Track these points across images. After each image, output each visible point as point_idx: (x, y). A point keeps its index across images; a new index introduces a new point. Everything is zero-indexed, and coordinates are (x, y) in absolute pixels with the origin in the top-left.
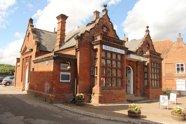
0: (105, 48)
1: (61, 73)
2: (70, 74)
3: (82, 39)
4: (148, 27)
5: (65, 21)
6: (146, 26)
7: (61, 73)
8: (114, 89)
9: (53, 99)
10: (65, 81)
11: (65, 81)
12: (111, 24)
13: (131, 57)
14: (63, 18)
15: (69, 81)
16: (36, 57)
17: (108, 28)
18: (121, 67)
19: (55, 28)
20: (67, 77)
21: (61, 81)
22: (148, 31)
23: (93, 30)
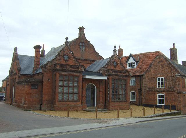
12: (71, 52)
14: (37, 48)
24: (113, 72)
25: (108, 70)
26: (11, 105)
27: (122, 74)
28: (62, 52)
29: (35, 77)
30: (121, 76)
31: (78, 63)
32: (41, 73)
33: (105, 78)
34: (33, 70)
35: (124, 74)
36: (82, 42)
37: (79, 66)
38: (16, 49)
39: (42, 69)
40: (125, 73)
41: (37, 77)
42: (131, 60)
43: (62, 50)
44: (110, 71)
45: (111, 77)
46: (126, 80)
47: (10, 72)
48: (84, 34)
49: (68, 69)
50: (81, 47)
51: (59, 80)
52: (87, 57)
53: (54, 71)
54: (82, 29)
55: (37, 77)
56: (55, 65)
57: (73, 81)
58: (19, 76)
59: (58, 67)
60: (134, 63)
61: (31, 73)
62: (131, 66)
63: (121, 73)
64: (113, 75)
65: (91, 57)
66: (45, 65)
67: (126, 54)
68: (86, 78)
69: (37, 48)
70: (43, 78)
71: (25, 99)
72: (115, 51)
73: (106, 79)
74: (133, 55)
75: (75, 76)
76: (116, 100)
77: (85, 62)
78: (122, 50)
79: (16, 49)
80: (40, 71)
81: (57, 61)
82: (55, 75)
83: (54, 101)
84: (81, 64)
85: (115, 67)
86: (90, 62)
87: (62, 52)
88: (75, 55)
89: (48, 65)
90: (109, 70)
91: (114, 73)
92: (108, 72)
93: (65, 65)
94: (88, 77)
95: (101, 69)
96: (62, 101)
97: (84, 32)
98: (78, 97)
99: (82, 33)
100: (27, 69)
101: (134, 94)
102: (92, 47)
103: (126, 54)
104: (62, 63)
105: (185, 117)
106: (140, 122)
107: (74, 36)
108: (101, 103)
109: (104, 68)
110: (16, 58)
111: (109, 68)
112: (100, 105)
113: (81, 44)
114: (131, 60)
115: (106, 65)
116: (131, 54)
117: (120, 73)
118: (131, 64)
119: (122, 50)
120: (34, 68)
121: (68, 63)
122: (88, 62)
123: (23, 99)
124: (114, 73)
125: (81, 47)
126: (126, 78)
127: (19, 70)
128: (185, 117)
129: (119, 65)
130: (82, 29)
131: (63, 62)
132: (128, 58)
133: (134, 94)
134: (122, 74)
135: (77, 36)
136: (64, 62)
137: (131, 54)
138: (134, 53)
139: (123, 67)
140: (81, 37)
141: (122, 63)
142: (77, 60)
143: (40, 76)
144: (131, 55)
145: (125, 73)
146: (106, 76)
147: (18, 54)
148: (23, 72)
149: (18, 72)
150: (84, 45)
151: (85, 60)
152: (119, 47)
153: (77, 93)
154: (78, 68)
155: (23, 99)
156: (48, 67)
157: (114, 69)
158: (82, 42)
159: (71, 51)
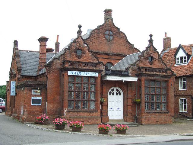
0: (72, 74)
1: (32, 98)
2: (41, 98)
3: (50, 66)
4: (151, 36)
5: (46, 43)
6: (152, 34)
7: (32, 98)
8: (83, 112)
9: (25, 119)
10: (36, 104)
11: (36, 104)
12: (86, 45)
13: (107, 79)
14: (43, 40)
15: (40, 104)
16: (114, 89)
17: (83, 49)
18: (166, 93)
19: (58, 36)
20: (38, 101)
21: (32, 104)
22: (151, 41)
23: (63, 56)
24: (146, 70)
25: (139, 69)
26: (10, 116)
27: (160, 74)
28: (74, 44)
29: (40, 79)
30: (158, 76)
31: (95, 59)
32: (44, 73)
33: (135, 79)
34: (37, 69)
35: (164, 74)
36: (109, 30)
37: (167, 70)
38: (16, 43)
39: (46, 69)
40: (166, 72)
41: (40, 80)
42: (181, 54)
43: (73, 42)
44: (142, 70)
45: (143, 78)
46: (166, 82)
47: (10, 73)
48: (112, 19)
49: (81, 68)
50: (107, 37)
51: (69, 83)
52: (116, 50)
53: (62, 71)
54: (108, 12)
55: (41, 78)
56: (64, 63)
57: (74, 84)
58: (20, 78)
59: (67, 65)
60: (185, 58)
61: (35, 74)
62: (181, 62)
63: (148, 71)
64: (148, 75)
65: (122, 50)
66: (50, 62)
67: (174, 45)
68: (108, 80)
69: (43, 40)
70: (47, 80)
71: (24, 108)
72: (79, 32)
73: (137, 81)
74: (184, 46)
75: (163, 81)
76: (152, 111)
77: (113, 57)
78: (170, 39)
79: (16, 43)
80: (44, 70)
81: (66, 58)
82: (63, 76)
83: (62, 110)
84: (100, 60)
85: (151, 63)
86: (120, 58)
87: (74, 44)
88: (91, 49)
89: (54, 63)
90: (142, 67)
91: (147, 72)
92: (140, 71)
93: (76, 62)
94: (109, 78)
95: (130, 67)
96: (72, 112)
97: (112, 16)
98: (96, 106)
99: (108, 17)
100: (30, 68)
101: (185, 101)
102: (123, 36)
103: (174, 45)
104: (74, 60)
105: (192, 135)
106: (175, 140)
107: (93, 21)
108: (130, 115)
109: (134, 65)
110: (17, 54)
111: (142, 65)
112: (128, 117)
113: (107, 32)
114: (181, 54)
115: (137, 61)
116: (180, 44)
117: (157, 71)
118: (181, 58)
119: (170, 39)
120: (38, 67)
121: (81, 60)
122: (117, 58)
123: (22, 108)
124: (147, 72)
125: (107, 37)
126: (166, 79)
127: (20, 70)
128: (192, 135)
129: (157, 61)
130: (108, 12)
131: (75, 59)
132: (177, 50)
133: (185, 101)
134: (160, 74)
135: (101, 22)
136: (76, 58)
137: (180, 44)
138: (185, 43)
139: (164, 63)
140: (107, 23)
141: (161, 58)
142: (95, 54)
143: (44, 78)
144: (180, 47)
145: (166, 72)
146: (136, 75)
147: (19, 49)
148: (25, 73)
149: (18, 73)
150: (111, 33)
151: (113, 55)
152: (166, 34)
153: (95, 100)
154: (95, 66)
155: (22, 108)
156: (54, 66)
157: (150, 66)
158: (109, 30)
159: (86, 44)
